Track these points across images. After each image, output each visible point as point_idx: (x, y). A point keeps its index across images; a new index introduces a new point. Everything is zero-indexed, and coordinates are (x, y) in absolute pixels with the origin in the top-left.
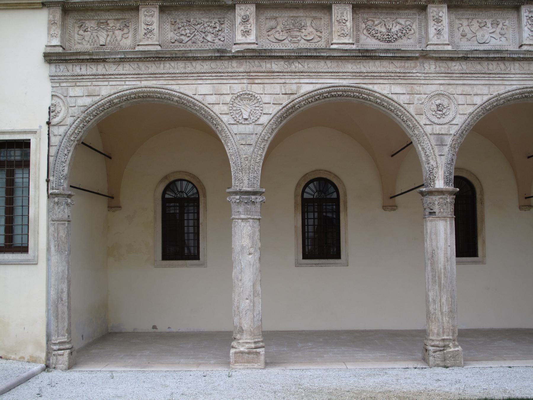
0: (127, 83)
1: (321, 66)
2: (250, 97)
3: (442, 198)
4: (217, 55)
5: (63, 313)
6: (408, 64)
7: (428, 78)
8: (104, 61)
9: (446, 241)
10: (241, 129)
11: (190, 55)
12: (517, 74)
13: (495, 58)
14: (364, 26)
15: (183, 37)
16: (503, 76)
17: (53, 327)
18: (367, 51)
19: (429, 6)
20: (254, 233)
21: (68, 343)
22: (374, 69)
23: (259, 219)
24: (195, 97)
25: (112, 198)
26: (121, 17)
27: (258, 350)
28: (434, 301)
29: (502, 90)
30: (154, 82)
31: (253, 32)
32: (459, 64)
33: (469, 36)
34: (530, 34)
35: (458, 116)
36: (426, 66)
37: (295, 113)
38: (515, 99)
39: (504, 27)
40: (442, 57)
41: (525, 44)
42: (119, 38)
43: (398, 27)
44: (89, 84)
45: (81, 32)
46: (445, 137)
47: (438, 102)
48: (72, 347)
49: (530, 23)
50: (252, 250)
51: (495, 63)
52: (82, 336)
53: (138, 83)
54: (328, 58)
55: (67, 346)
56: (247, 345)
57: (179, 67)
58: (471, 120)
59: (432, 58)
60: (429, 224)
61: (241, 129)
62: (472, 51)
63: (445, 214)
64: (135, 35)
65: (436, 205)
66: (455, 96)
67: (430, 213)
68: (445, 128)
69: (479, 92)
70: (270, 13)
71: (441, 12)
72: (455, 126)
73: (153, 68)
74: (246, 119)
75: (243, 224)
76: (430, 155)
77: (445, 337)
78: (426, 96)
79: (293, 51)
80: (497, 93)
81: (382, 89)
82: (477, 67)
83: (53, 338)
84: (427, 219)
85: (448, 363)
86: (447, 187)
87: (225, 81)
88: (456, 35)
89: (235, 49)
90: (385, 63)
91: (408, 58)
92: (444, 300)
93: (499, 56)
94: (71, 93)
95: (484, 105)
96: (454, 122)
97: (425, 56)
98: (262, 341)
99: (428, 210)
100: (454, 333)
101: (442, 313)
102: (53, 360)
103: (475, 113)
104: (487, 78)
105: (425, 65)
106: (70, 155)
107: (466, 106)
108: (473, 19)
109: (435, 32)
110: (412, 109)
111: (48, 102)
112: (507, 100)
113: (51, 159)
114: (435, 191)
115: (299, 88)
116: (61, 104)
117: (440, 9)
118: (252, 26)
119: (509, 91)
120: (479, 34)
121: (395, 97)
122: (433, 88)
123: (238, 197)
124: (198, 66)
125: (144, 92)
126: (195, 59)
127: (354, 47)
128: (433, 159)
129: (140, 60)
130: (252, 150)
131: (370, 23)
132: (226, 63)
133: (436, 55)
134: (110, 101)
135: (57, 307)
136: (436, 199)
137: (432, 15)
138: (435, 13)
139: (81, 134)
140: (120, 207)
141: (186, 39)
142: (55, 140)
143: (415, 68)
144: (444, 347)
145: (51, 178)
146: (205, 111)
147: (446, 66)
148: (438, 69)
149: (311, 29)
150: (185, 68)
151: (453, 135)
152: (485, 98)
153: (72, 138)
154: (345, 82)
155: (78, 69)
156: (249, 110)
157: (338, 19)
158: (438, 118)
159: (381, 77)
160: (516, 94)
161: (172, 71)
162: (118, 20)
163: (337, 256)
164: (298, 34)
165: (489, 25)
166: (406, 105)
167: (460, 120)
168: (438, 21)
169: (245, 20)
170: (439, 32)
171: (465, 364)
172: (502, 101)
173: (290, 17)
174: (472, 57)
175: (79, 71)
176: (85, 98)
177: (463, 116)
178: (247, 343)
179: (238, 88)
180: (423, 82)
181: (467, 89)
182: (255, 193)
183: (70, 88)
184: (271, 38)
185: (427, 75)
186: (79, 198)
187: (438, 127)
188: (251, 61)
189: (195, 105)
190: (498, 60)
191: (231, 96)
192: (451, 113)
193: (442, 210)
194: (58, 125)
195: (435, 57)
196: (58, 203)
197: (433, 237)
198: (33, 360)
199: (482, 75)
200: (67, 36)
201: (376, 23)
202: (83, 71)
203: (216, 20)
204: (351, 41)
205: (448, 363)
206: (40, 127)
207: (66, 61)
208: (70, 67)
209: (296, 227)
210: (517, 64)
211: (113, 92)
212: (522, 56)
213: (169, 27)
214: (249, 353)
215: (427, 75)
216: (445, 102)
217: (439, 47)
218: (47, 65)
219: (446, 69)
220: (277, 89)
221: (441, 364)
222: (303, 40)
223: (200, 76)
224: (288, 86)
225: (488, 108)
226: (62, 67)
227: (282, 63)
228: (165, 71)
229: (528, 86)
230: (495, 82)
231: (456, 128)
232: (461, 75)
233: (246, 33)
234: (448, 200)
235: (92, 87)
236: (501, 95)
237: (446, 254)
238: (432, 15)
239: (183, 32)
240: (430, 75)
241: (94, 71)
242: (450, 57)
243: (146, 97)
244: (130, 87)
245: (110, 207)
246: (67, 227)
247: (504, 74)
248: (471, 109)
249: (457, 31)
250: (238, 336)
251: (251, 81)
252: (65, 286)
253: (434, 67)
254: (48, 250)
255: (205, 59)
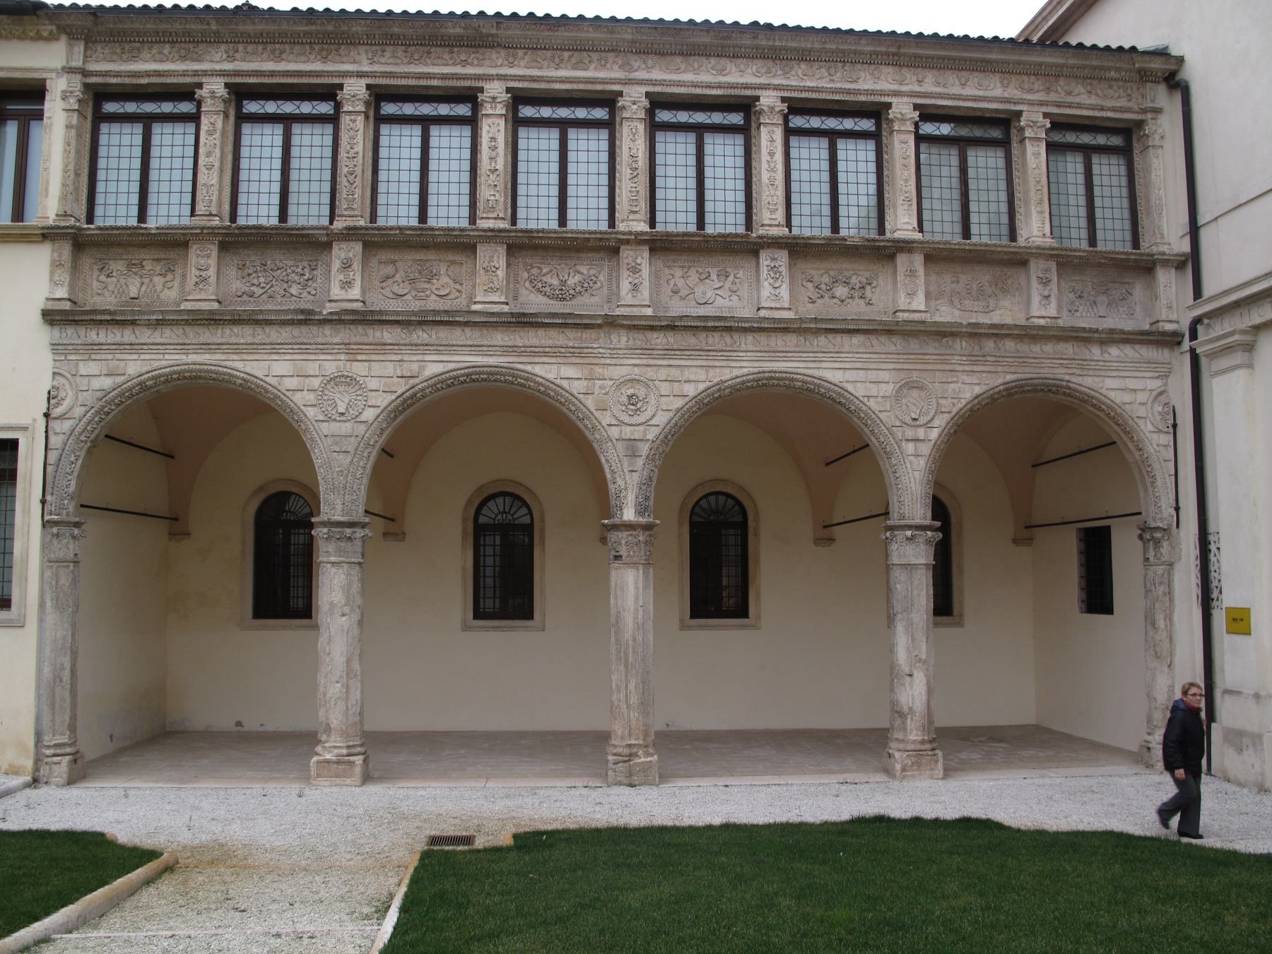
0: (167, 357)
1: (457, 336)
2: (350, 381)
4: (300, 317)
5: (63, 700)
6: (587, 334)
8: (133, 323)
9: (637, 598)
10: (334, 428)
11: (260, 317)
14: (526, 275)
15: (254, 289)
17: (46, 721)
18: (524, 315)
20: (350, 585)
21: (70, 745)
22: (535, 341)
23: (360, 564)
24: (267, 379)
25: (176, 519)
26: (163, 256)
27: (352, 758)
28: (618, 687)
29: (727, 375)
30: (208, 356)
31: (358, 283)
33: (684, 292)
35: (660, 413)
36: (614, 337)
37: (418, 405)
42: (159, 288)
43: (578, 278)
44: (110, 357)
45: (103, 278)
46: (639, 443)
47: (630, 391)
48: (77, 752)
50: (346, 609)
51: (717, 335)
52: (111, 737)
53: (184, 357)
54: (466, 324)
55: (68, 750)
56: (336, 751)
57: (244, 334)
59: (622, 326)
60: (613, 574)
61: (334, 428)
62: (681, 318)
64: (183, 284)
69: (692, 377)
70: (385, 255)
73: (205, 335)
74: (342, 414)
75: (333, 570)
77: (633, 742)
79: (414, 313)
81: (547, 371)
82: (690, 340)
83: (46, 738)
85: (635, 779)
87: (312, 357)
89: (329, 308)
90: (553, 333)
91: (587, 326)
92: (632, 686)
94: (83, 372)
96: (653, 422)
97: (611, 323)
98: (361, 746)
100: (646, 735)
101: (628, 706)
102: (44, 771)
106: (80, 462)
109: (629, 286)
110: (590, 402)
111: (47, 384)
112: (735, 389)
113: (49, 469)
115: (422, 368)
116: (67, 386)
118: (356, 275)
120: (699, 291)
121: (565, 384)
122: (623, 371)
123: (325, 530)
124: (274, 334)
125: (191, 371)
126: (269, 323)
127: (506, 309)
129: (187, 323)
130: (349, 459)
131: (535, 271)
132: (314, 329)
134: (140, 384)
135: (53, 691)
136: (623, 536)
139: (97, 432)
140: (188, 534)
141: (258, 291)
142: (55, 441)
143: (597, 342)
144: (630, 755)
145: (48, 498)
146: (281, 400)
148: (631, 342)
149: (447, 280)
150: (253, 335)
152: (702, 387)
153: (83, 438)
154: (492, 361)
155: (93, 335)
156: (347, 401)
157: (485, 265)
159: (545, 354)
160: (749, 381)
161: (233, 340)
162: (158, 260)
163: (530, 616)
164: (426, 286)
165: (714, 277)
166: (581, 396)
167: (662, 419)
168: (635, 270)
169: (347, 266)
170: (635, 288)
171: (661, 783)
173: (414, 260)
175: (95, 337)
176: (103, 378)
178: (335, 747)
179: (331, 368)
180: (608, 361)
182: (351, 525)
183: (81, 364)
184: (387, 292)
186: (96, 526)
187: (629, 429)
188: (352, 327)
189: (267, 391)
191: (321, 378)
194: (61, 417)
196: (57, 535)
197: (619, 593)
198: (13, 771)
200: (81, 283)
201: (545, 271)
202: (102, 338)
203: (305, 263)
204: (503, 299)
205: (635, 779)
206: (35, 420)
207: (76, 322)
208: (82, 331)
209: (464, 569)
210: (750, 337)
211: (145, 369)
213: (234, 273)
214: (338, 763)
216: (641, 392)
218: (47, 328)
220: (389, 369)
221: (625, 781)
222: (433, 297)
223: (275, 348)
224: (405, 365)
226: (70, 330)
227: (399, 330)
228: (223, 340)
230: (717, 364)
231: (656, 431)
233: (347, 284)
235: (115, 362)
237: (636, 618)
239: (255, 281)
241: (118, 339)
243: (195, 377)
244: (170, 363)
245: (173, 535)
246: (73, 572)
248: (679, 403)
250: (324, 738)
251: (351, 357)
252: (66, 661)
253: (625, 339)
254: (42, 605)
255: (283, 323)
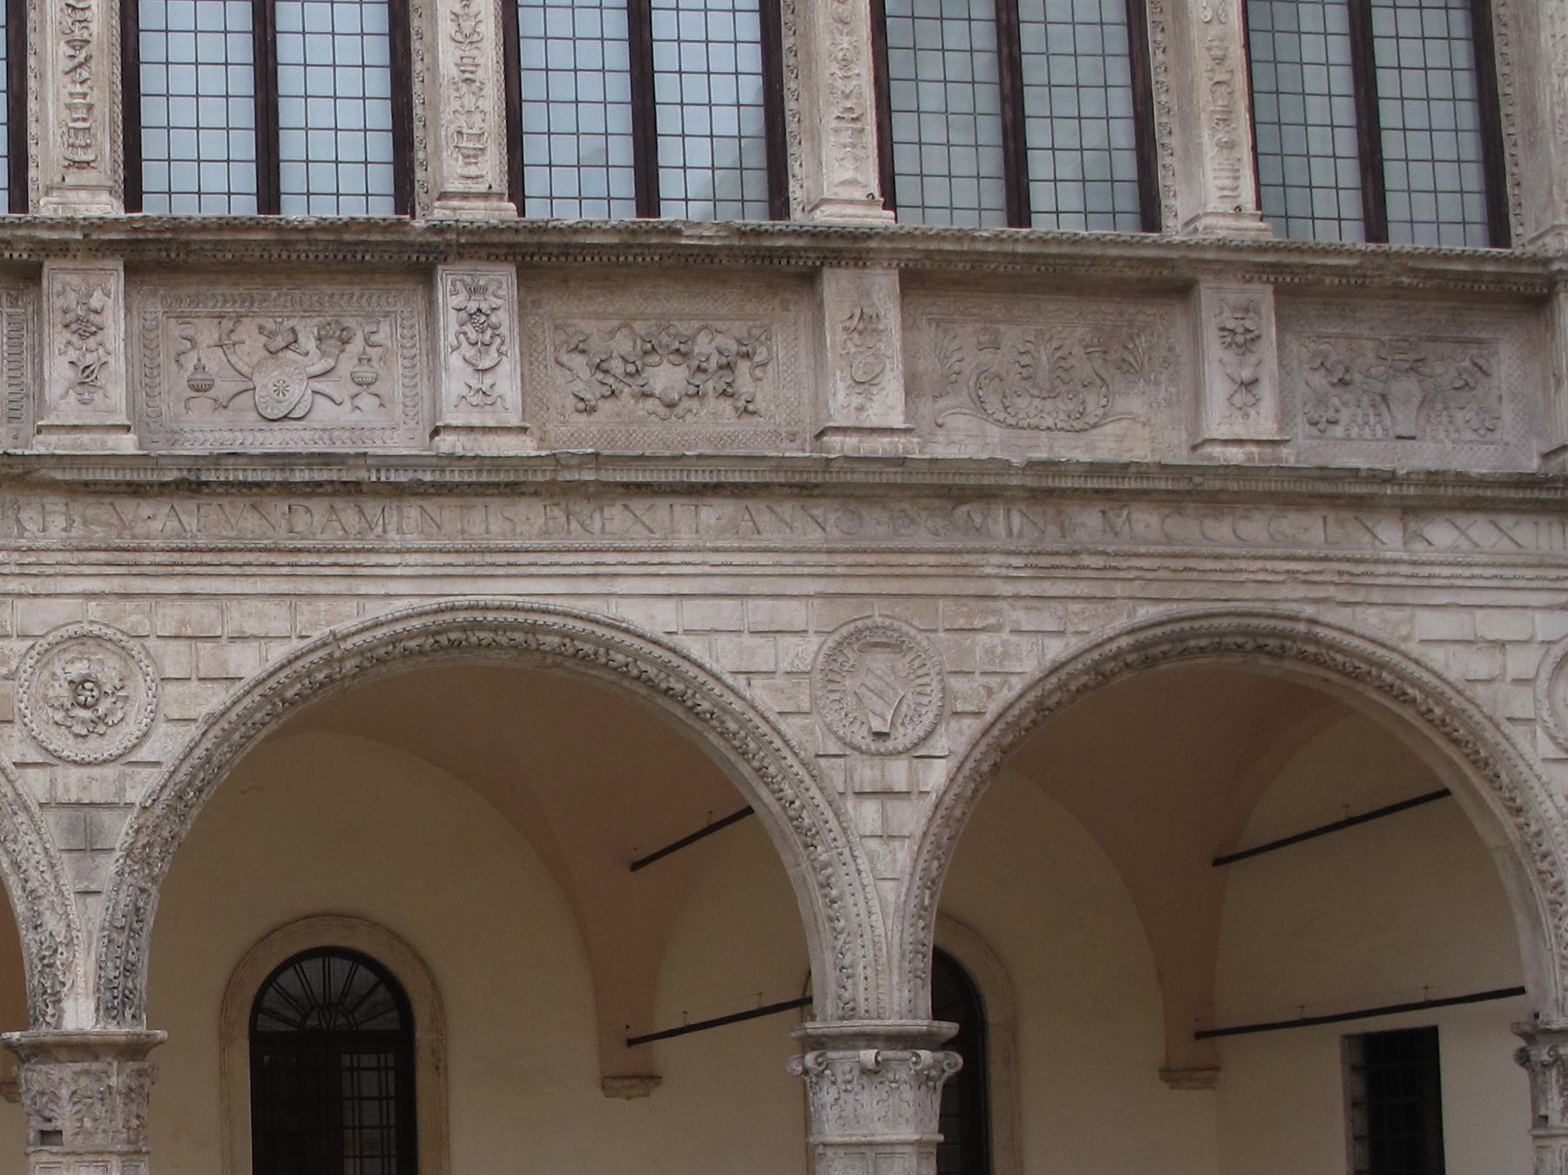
3: (86, 1072)
7: (35, 570)
12: (409, 551)
13: (320, 484)
16: (351, 559)
19: (48, 266)
29: (348, 618)
32: (167, 509)
33: (223, 389)
34: (475, 384)
35: (162, 728)
38: (408, 654)
39: (372, 352)
40: (95, 483)
41: (447, 428)
47: (78, 669)
49: (473, 336)
51: (319, 506)
58: (217, 746)
59: (53, 486)
62: (217, 460)
63: (99, 1140)
65: (64, 1102)
66: (148, 643)
67: (43, 1133)
68: (104, 779)
69: (251, 627)
71: (98, 294)
72: (145, 772)
76: (41, 892)
78: (30, 643)
80: (327, 631)
82: (247, 522)
84: (33, 1159)
86: (112, 1028)
88: (165, 386)
93: (334, 476)
95: (272, 683)
96: (142, 754)
99: (37, 1124)
103: (233, 716)
104: (285, 570)
105: (23, 516)
107: (194, 685)
108: (239, 318)
109: (70, 373)
114: (58, 1045)
117: (93, 280)
119: (378, 624)
120: (265, 382)
122: (59, 611)
128: (53, 909)
133: (69, 476)
136: (63, 1076)
137: (59, 303)
138: (73, 296)
147: (115, 521)
148: (77, 531)
151: (136, 810)
158: (77, 736)
160: (411, 635)
165: (308, 342)
167: (167, 745)
168: (85, 327)
170: (87, 377)
172: (350, 665)
174: (221, 484)
177: (180, 728)
181: (201, 616)
185: (32, 558)
187: (75, 773)
190: (334, 494)
192: (131, 718)
193: (88, 1123)
195: (66, 482)
199: (264, 558)
210: (413, 511)
212: (428, 477)
215: (32, 558)
216: (108, 670)
217: (86, 438)
219: (114, 532)
225: (290, 693)
229: (482, 600)
230: (320, 587)
231: (154, 778)
232: (176, 557)
234: (114, 1081)
236: (345, 637)
238: (59, 303)
240: (46, 558)
242: (129, 484)
247: (357, 551)
248: (215, 699)
249: (174, 367)
253: (61, 522)
